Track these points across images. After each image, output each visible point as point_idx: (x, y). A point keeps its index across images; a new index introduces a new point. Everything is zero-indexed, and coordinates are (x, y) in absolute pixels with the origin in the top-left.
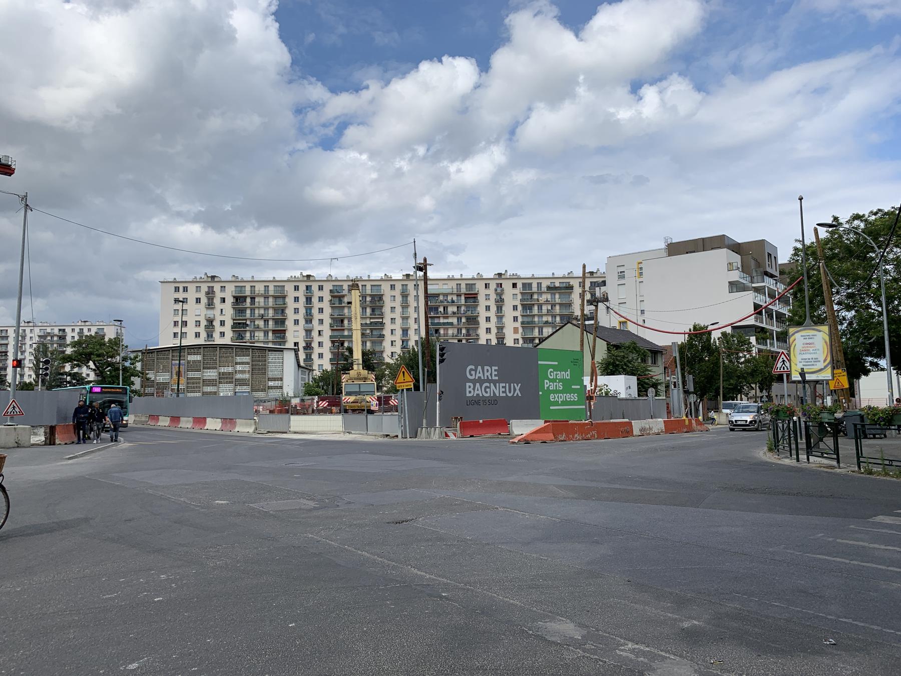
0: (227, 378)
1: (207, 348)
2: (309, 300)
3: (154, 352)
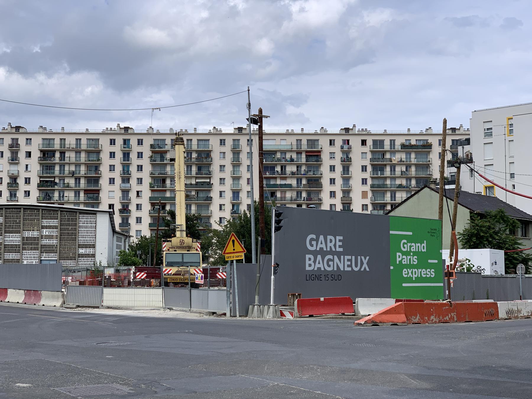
2: (126, 155)
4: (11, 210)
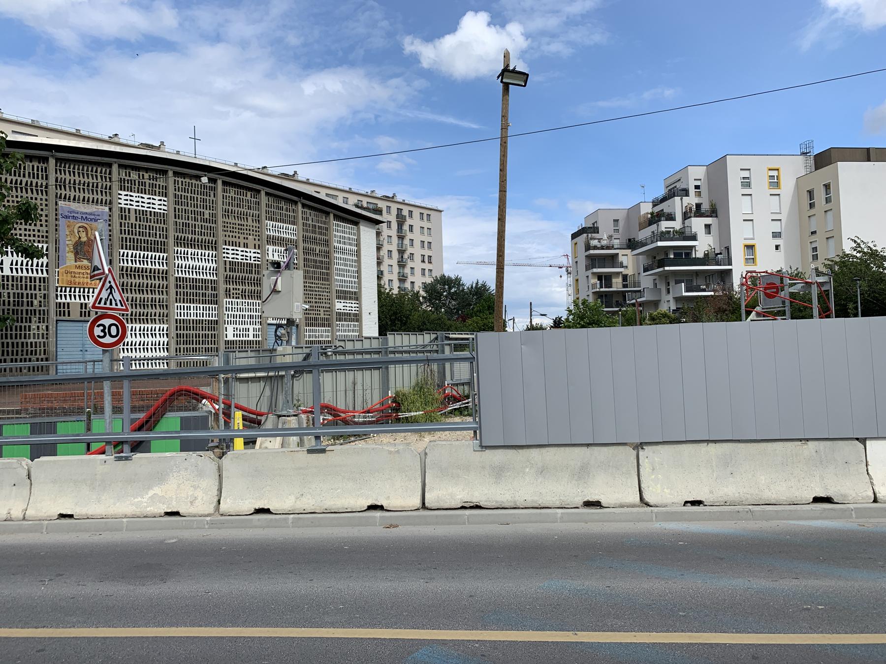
0: (243, 281)
1: (184, 175)
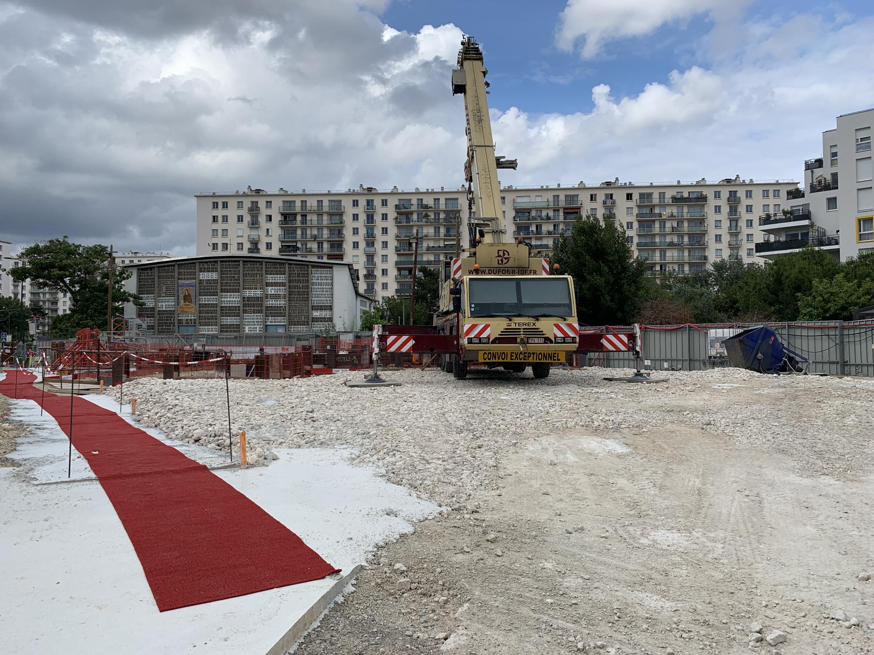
1: (226, 261)
2: (370, 218)
3: (154, 268)
4: (228, 263)
